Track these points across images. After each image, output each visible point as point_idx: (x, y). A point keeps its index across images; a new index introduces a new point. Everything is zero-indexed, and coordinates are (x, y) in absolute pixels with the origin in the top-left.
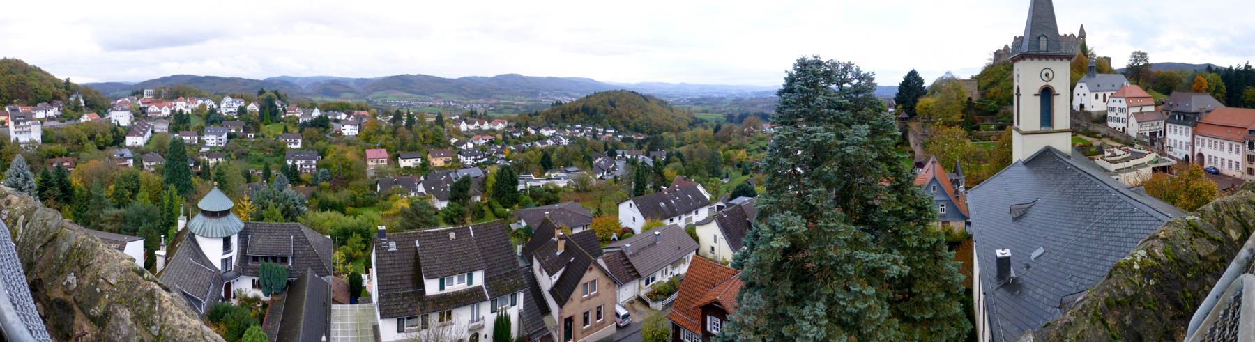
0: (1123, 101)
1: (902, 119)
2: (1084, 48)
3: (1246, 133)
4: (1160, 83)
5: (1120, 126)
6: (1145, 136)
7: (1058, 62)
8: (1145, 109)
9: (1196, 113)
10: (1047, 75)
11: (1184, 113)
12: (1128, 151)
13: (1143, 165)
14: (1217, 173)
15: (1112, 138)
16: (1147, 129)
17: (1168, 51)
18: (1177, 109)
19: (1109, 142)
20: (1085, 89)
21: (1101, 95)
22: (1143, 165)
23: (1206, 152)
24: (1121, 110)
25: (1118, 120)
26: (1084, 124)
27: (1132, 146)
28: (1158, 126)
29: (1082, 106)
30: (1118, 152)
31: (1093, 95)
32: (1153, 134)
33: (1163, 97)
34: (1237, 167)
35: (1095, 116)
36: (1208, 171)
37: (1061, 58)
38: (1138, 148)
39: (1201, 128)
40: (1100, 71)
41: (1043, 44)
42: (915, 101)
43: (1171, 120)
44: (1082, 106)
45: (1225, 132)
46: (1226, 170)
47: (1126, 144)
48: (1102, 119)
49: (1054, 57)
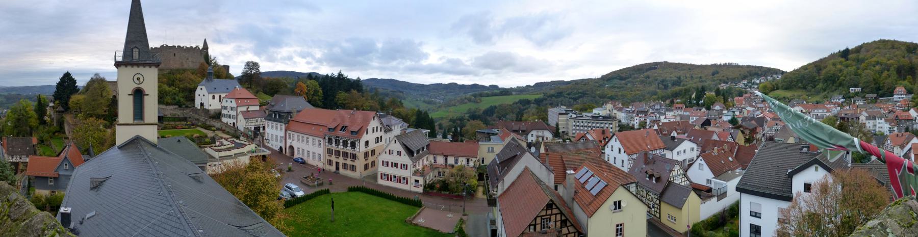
0: (234, 101)
1: (59, 112)
2: (207, 57)
5: (230, 121)
7: (147, 68)
8: (251, 108)
9: (289, 113)
10: (138, 79)
11: (279, 112)
12: (232, 142)
13: (243, 154)
14: (304, 163)
15: (224, 131)
16: (252, 124)
18: (276, 108)
19: (220, 134)
20: (205, 91)
21: (217, 96)
22: (243, 154)
24: (232, 109)
25: (229, 116)
26: (202, 119)
27: (238, 138)
28: (259, 122)
29: (202, 104)
30: (225, 142)
31: (211, 96)
32: (257, 129)
33: (268, 98)
34: (319, 158)
35: (212, 113)
36: (296, 161)
37: (150, 65)
38: (243, 140)
40: (218, 77)
42: (69, 98)
43: (269, 118)
44: (202, 104)
45: (309, 128)
46: (310, 161)
47: (233, 136)
48: (218, 115)
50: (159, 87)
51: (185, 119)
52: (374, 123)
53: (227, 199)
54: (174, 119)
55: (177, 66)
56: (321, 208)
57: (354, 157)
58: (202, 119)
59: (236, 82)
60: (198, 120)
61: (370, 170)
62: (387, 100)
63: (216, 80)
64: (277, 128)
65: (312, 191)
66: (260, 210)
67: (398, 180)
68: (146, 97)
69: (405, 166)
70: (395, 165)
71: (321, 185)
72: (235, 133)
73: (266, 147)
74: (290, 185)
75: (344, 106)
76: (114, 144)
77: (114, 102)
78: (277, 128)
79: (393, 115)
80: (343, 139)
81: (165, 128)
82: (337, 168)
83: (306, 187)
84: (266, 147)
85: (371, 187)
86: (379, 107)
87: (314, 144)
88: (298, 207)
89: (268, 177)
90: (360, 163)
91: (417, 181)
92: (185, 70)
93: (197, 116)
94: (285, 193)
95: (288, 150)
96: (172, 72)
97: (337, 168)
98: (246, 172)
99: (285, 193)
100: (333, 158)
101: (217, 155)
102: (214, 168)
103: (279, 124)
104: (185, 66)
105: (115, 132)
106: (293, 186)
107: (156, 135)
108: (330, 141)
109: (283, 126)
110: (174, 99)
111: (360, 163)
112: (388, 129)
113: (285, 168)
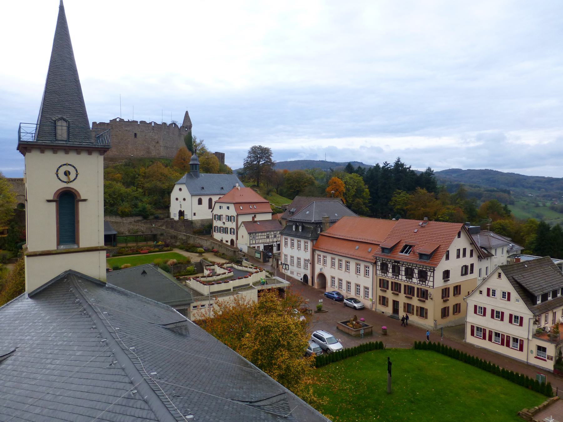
0: (232, 207)
2: (189, 140)
3: (378, 251)
4: (274, 181)
5: (227, 238)
6: (257, 251)
7: (84, 157)
8: (259, 218)
9: (318, 224)
10: (67, 173)
12: (230, 269)
13: (247, 287)
14: (340, 299)
16: (261, 243)
17: (291, 145)
18: (296, 217)
19: (211, 258)
21: (205, 200)
22: (247, 287)
23: (329, 272)
24: (229, 218)
25: (225, 230)
26: (182, 236)
27: (239, 263)
29: (181, 213)
31: (196, 199)
32: (269, 248)
33: (285, 202)
34: (366, 294)
36: (329, 297)
37: (90, 150)
38: (246, 266)
39: (324, 243)
40: (208, 170)
41: (62, 131)
44: (181, 213)
47: (232, 261)
48: (207, 229)
49: (78, 150)
50: (105, 186)
51: (154, 238)
52: (461, 243)
53: (222, 356)
54: (136, 238)
55: (141, 154)
56: (372, 371)
57: (424, 295)
58: (182, 236)
59: (235, 176)
60: (175, 237)
61: (452, 318)
62: (481, 205)
63: (203, 175)
64: (299, 247)
65: (354, 344)
66: (277, 372)
67: (505, 341)
68: (81, 205)
69: (517, 320)
70: (498, 315)
71: (369, 335)
72: (233, 256)
73: (283, 276)
74: (321, 333)
75: (404, 214)
76: (23, 290)
77: (20, 215)
78: (299, 247)
79: (492, 229)
80: (404, 266)
81: (120, 254)
82: (396, 310)
83: (345, 338)
84: (283, 276)
85: (454, 346)
86: (465, 216)
87: (358, 271)
88: (332, 367)
89: (290, 321)
90: (433, 306)
91: (541, 349)
92: (153, 160)
93: (172, 232)
94: (313, 346)
95: (316, 281)
96: (131, 163)
97: (396, 310)
98: (256, 315)
99: (313, 346)
100: (389, 295)
101: (205, 290)
102: (204, 310)
103: (302, 241)
104: (154, 154)
105: (22, 269)
106: (326, 335)
107: (104, 265)
108: (384, 268)
109: (310, 244)
110: (136, 206)
111: (433, 306)
112: (484, 254)
113: (313, 307)
